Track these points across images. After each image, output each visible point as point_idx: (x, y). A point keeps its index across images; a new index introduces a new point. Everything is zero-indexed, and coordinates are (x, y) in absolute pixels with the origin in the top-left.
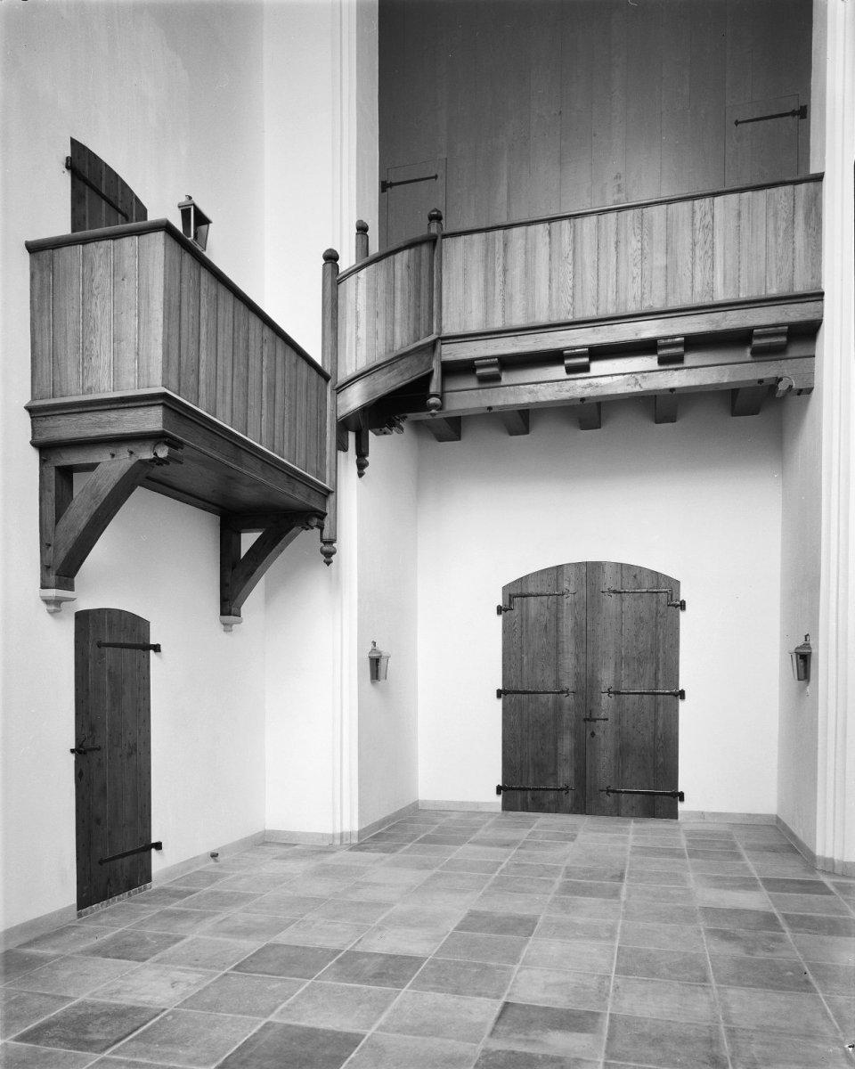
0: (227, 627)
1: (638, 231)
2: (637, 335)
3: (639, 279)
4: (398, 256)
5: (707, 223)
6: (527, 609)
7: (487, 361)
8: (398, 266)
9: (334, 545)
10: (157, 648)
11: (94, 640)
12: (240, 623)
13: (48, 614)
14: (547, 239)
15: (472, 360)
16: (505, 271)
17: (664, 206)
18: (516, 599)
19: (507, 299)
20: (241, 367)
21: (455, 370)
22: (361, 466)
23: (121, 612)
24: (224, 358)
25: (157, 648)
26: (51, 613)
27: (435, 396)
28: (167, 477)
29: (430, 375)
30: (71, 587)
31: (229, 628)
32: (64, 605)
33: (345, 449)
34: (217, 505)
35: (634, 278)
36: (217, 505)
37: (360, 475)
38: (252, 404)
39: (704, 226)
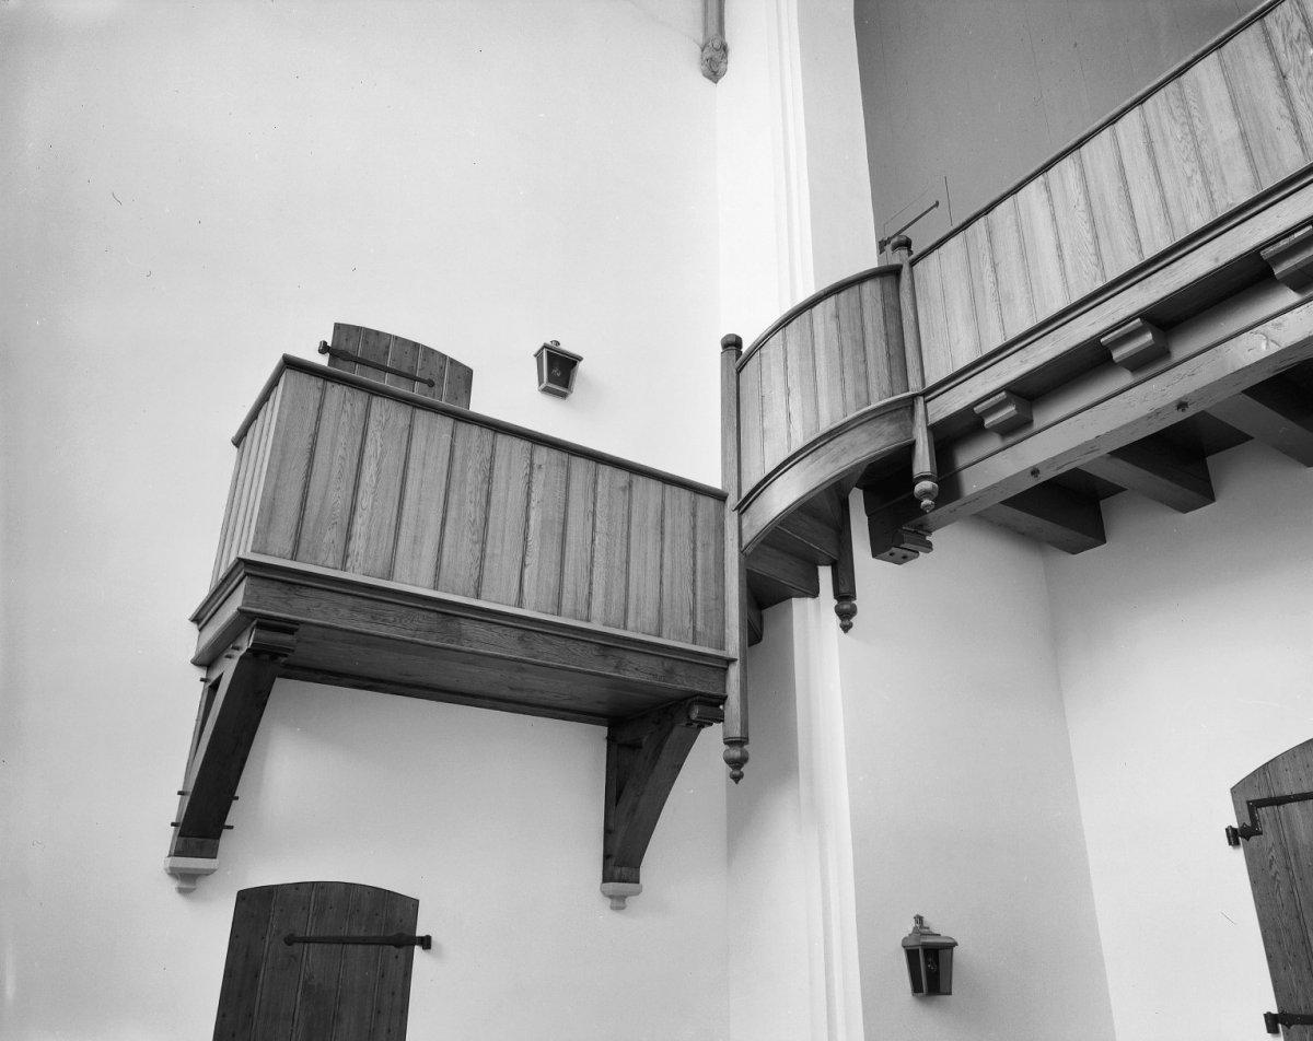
0: (618, 902)
1: (1177, 113)
2: (1217, 260)
3: (1198, 177)
4: (818, 309)
5: (1295, 36)
6: (1292, 833)
7: (994, 402)
8: (819, 329)
9: (745, 747)
10: (426, 943)
11: (279, 932)
12: (638, 893)
13: (178, 895)
14: (1044, 195)
15: (970, 408)
16: (995, 266)
17: (1214, 55)
18: (1262, 812)
19: (1001, 300)
20: (470, 508)
21: (953, 435)
22: (846, 615)
23: (349, 886)
24: (610, 518)
25: (426, 943)
26: (181, 891)
27: (925, 478)
28: (411, 678)
29: (912, 446)
30: (212, 854)
31: (621, 905)
32: (629, 900)
33: (814, 593)
34: (604, 716)
35: (1189, 179)
36: (604, 716)
37: (846, 628)
38: (497, 551)
39: (1291, 42)
